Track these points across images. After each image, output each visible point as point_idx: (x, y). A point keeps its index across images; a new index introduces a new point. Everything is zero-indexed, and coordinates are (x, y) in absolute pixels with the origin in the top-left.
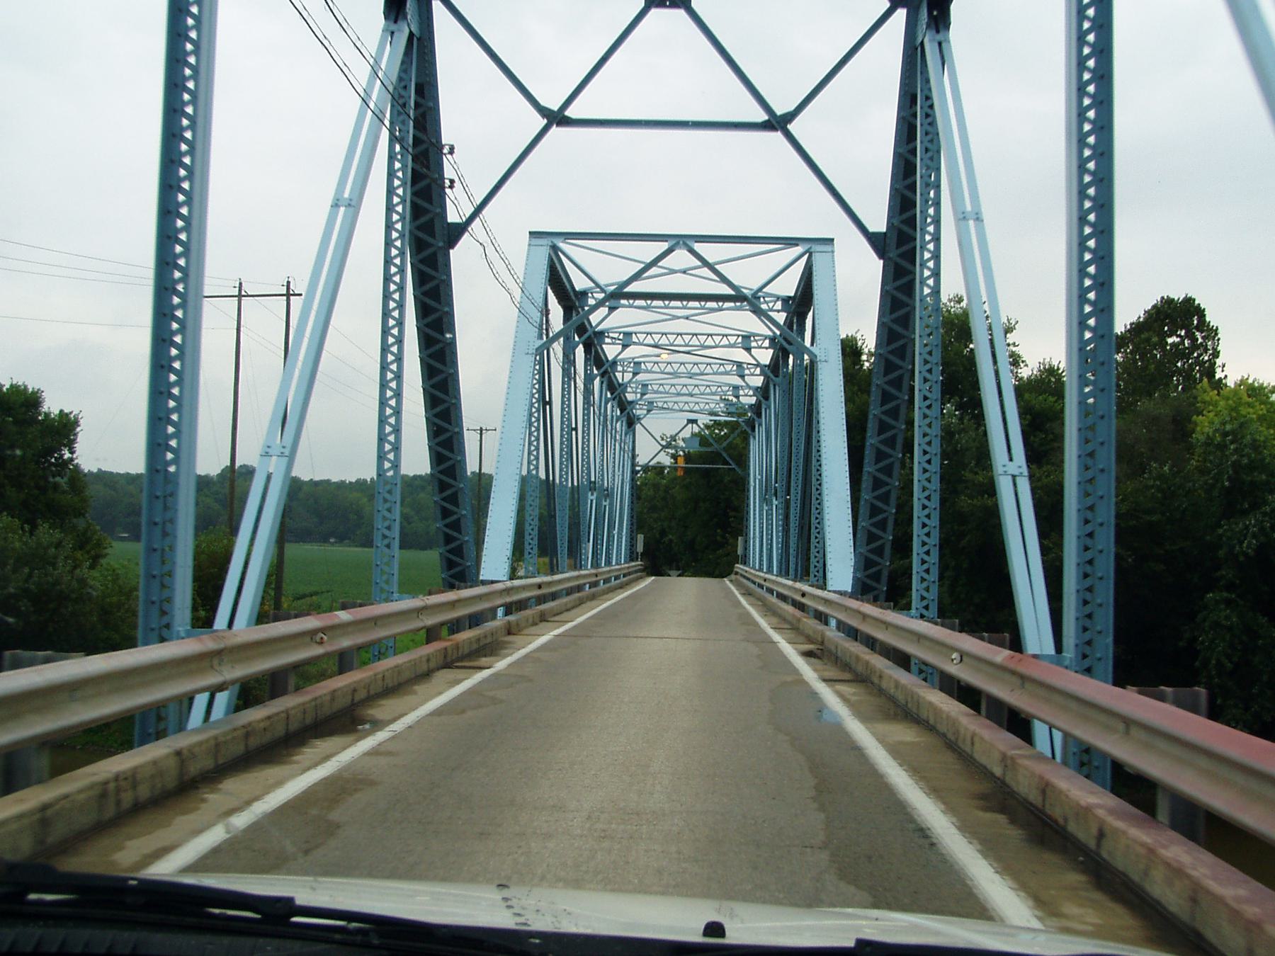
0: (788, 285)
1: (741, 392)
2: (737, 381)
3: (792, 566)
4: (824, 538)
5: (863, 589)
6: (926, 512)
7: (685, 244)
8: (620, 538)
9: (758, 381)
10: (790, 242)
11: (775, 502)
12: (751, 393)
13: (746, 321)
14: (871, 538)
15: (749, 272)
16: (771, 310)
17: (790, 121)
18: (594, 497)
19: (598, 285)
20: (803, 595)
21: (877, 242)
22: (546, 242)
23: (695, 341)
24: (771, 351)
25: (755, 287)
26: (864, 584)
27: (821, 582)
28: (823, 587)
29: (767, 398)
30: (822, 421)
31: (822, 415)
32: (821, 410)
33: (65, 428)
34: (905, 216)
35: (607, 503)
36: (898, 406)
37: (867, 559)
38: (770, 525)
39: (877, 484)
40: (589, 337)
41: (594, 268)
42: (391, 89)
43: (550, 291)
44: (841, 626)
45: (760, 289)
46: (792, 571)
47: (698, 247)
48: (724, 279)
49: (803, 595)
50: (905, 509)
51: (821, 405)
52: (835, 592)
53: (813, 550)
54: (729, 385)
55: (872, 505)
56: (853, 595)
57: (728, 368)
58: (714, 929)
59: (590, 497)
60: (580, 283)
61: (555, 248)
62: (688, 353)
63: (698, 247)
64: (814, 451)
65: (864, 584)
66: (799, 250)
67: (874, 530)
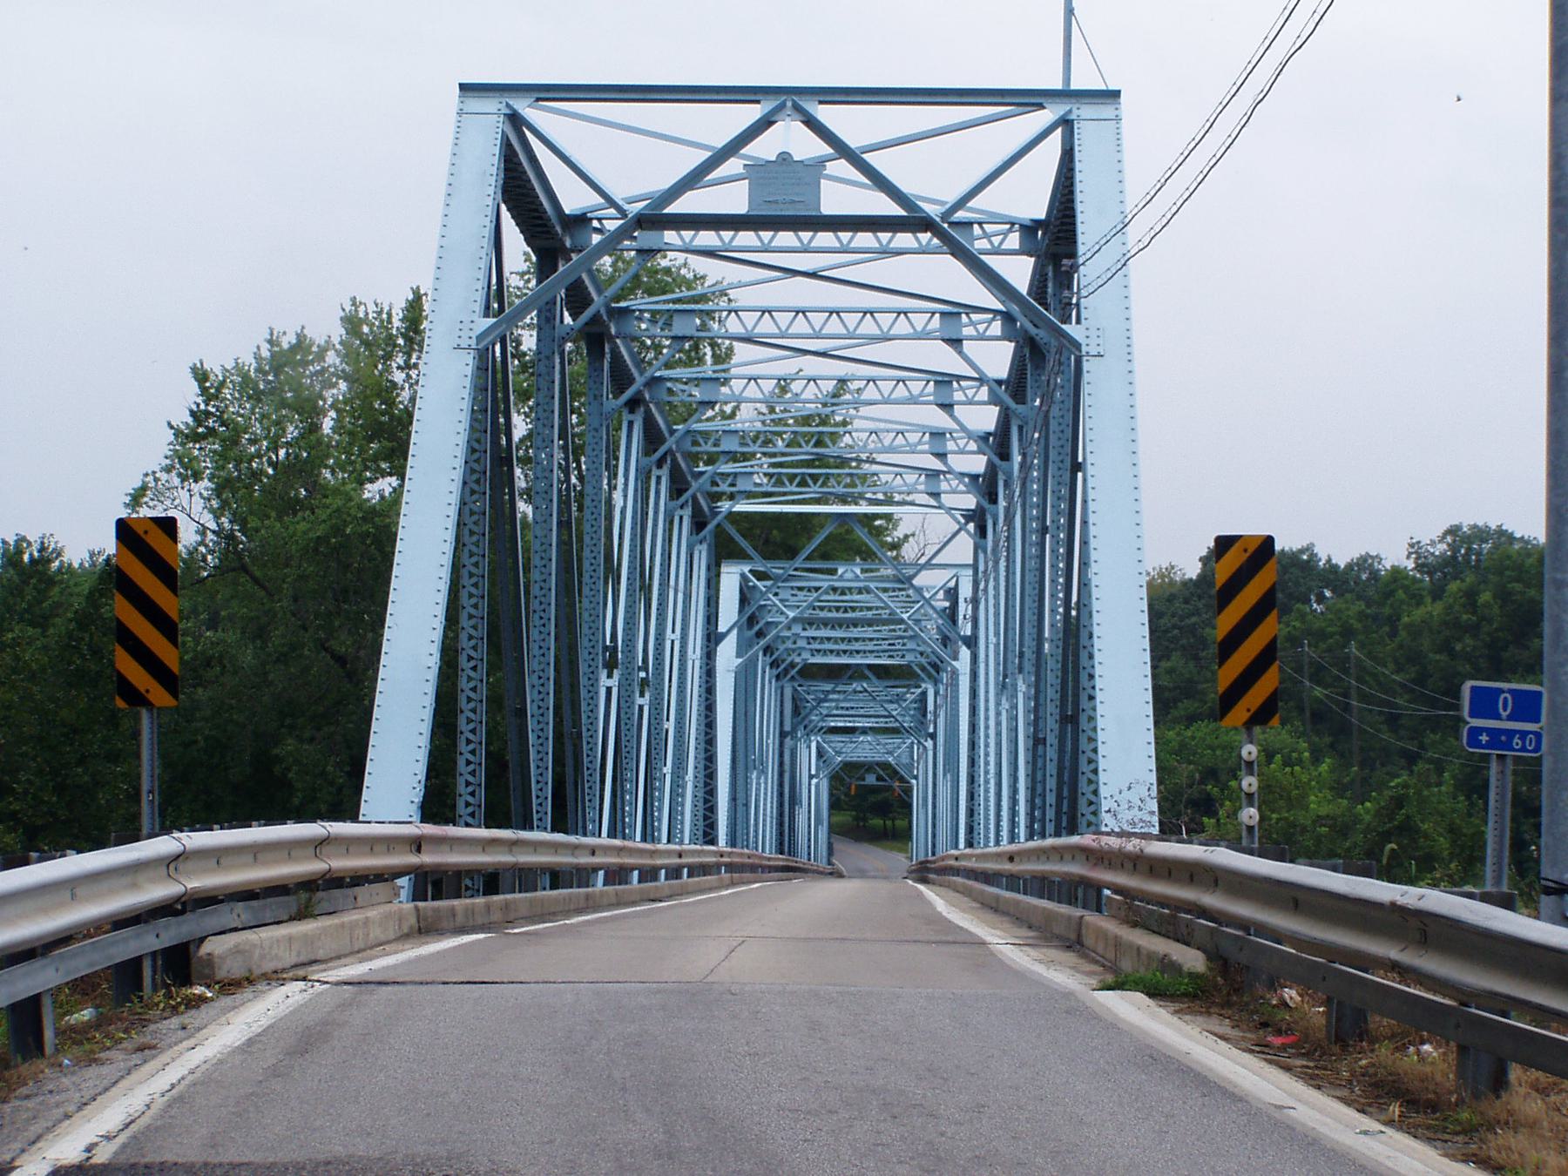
0: (1028, 194)
1: (951, 446)
2: (940, 419)
7: (798, 109)
8: (678, 784)
9: (986, 418)
10: (1029, 99)
11: (1022, 687)
12: (984, 393)
13: (949, 278)
15: (934, 171)
16: (997, 252)
18: (613, 682)
19: (611, 202)
22: (492, 105)
23: (834, 326)
24: (1009, 348)
25: (951, 198)
28: (1094, 827)
29: (1005, 456)
35: (645, 701)
40: (596, 318)
41: (607, 164)
42: (710, 979)
43: (506, 215)
45: (961, 203)
47: (826, 114)
48: (880, 182)
50: (1020, 440)
54: (923, 430)
57: (916, 387)
59: (604, 681)
60: (572, 197)
61: (515, 120)
62: (824, 354)
63: (826, 114)
66: (1046, 116)
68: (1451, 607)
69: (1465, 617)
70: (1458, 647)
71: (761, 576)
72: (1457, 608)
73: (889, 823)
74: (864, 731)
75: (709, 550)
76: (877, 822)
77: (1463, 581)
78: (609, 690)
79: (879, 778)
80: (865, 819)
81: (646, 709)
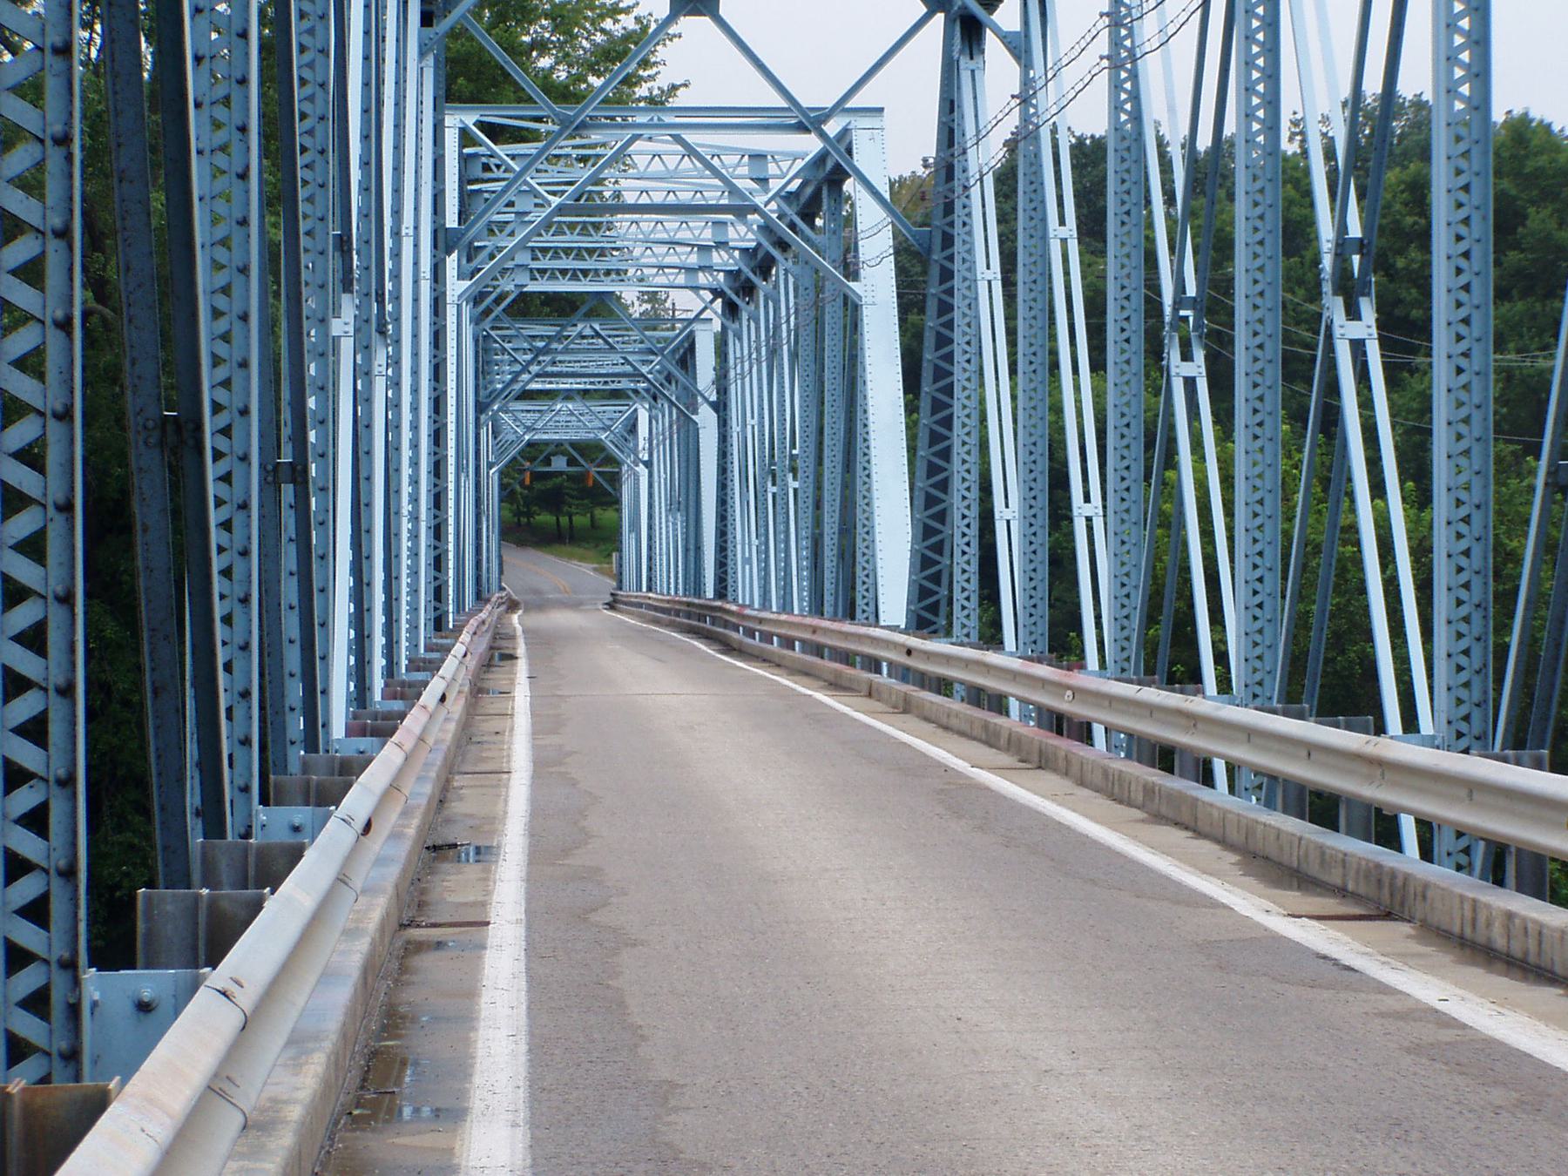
3: (828, 599)
4: (875, 570)
6: (966, 594)
17: (825, 122)
18: (1366, 327)
20: (909, 652)
26: (920, 618)
27: (872, 618)
28: (876, 624)
30: (871, 410)
31: (870, 402)
33: (1549, 125)
34: (944, 287)
36: (938, 602)
37: (926, 526)
53: (860, 588)
55: (938, 333)
58: (198, 813)
59: (1346, 331)
64: (859, 439)
68: (1388, 206)
69: (1409, 220)
70: (1400, 263)
71: (496, 132)
72: (1398, 207)
73: (564, 520)
74: (568, 395)
75: (436, 67)
76: (545, 518)
77: (1405, 168)
78: (1190, 383)
79: (572, 462)
80: (529, 515)
81: (1098, 524)
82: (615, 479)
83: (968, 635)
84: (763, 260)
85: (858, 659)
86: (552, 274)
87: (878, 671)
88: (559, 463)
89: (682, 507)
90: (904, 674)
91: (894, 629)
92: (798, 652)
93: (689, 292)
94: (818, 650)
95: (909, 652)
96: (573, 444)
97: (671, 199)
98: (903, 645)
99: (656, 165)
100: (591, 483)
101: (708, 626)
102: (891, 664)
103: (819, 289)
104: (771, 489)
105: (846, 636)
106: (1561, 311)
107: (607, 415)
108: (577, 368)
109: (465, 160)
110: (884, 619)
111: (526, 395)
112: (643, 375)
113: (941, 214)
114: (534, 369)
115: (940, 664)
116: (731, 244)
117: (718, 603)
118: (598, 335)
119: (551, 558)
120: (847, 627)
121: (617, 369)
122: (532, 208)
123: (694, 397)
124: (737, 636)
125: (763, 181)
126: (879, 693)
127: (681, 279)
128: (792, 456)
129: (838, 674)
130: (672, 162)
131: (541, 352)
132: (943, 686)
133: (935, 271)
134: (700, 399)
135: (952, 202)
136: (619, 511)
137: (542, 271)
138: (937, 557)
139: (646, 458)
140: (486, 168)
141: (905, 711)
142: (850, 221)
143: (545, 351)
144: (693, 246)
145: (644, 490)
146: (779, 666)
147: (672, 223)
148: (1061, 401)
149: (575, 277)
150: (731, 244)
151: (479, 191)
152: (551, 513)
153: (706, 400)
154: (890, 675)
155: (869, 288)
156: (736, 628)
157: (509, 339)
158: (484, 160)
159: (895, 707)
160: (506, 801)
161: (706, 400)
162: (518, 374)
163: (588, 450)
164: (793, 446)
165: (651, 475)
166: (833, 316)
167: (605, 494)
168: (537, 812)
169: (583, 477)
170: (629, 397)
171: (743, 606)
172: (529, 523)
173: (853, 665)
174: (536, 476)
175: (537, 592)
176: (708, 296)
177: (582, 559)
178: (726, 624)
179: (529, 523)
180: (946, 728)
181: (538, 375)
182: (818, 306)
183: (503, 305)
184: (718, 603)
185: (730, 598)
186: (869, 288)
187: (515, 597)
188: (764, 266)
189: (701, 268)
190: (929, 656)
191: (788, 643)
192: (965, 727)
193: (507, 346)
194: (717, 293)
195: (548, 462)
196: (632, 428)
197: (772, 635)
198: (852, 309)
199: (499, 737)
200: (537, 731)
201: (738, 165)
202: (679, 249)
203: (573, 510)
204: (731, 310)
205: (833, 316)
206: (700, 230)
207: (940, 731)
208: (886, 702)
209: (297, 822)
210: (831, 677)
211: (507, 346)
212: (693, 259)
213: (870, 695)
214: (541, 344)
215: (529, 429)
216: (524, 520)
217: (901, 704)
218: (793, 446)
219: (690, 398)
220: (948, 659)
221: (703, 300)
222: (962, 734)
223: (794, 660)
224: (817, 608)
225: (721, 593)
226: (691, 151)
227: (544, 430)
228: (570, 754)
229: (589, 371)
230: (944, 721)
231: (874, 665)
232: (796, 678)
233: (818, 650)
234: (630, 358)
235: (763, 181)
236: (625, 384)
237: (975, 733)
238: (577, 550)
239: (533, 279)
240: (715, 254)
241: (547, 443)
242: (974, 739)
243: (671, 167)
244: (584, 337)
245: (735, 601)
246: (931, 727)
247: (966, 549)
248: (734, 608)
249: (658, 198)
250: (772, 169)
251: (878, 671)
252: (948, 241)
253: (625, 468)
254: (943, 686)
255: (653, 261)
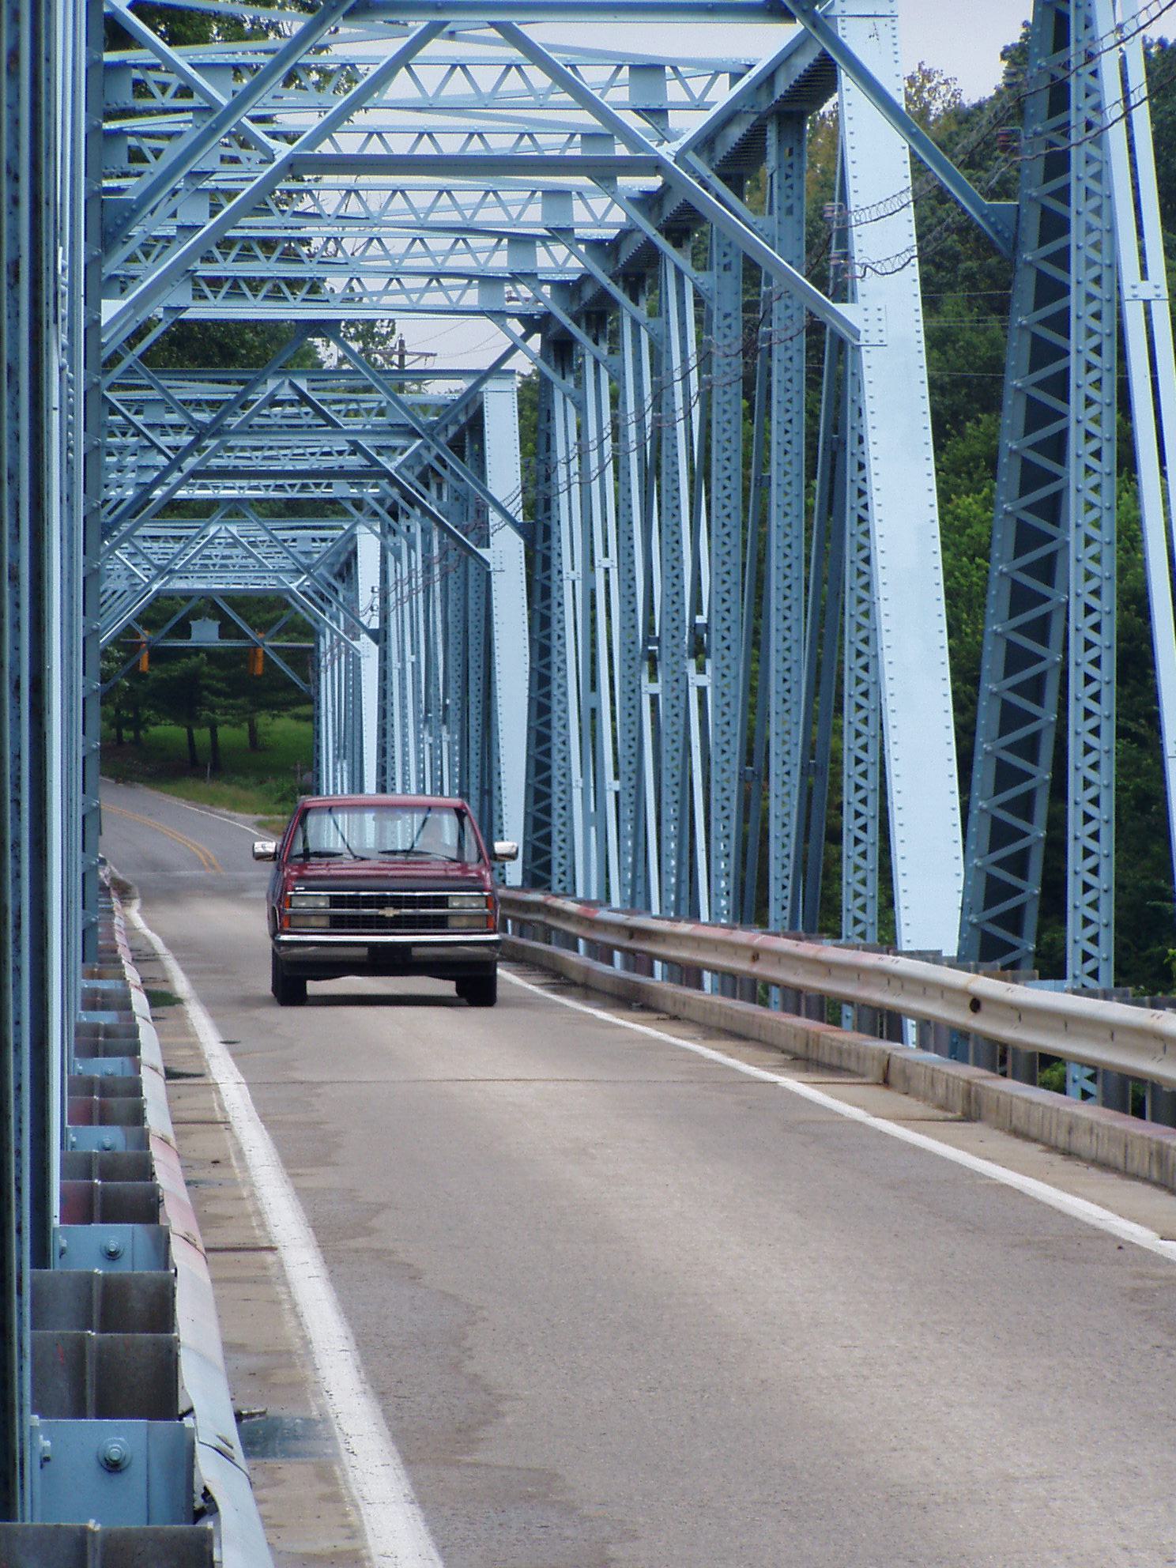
5: (987, 947)
11: (445, 736)
14: (1001, 834)
20: (976, 1005)
21: (521, 529)
28: (888, 941)
32: (869, 406)
37: (991, 880)
38: (436, 768)
39: (1011, 718)
44: (930, 1032)
46: (779, 893)
49: (755, 958)
51: (868, 390)
52: (911, 955)
56: (959, 962)
65: (534, 875)
67: (1005, 816)
73: (202, 735)
74: (235, 509)
76: (167, 731)
79: (227, 629)
80: (137, 724)
82: (306, 661)
83: (863, 935)
84: (633, 260)
85: (848, 1011)
86: (236, 288)
87: (896, 1034)
88: (205, 633)
89: (454, 716)
90: (957, 1043)
91: (934, 957)
92: (708, 990)
93: (486, 323)
94: (755, 990)
95: (755, 958)
96: (230, 597)
97: (476, 147)
98: (964, 992)
99: (458, 85)
100: (259, 668)
101: (510, 935)
102: (926, 1024)
103: (754, 312)
104: (648, 688)
105: (829, 968)
106: (927, 315)
107: (301, 546)
108: (257, 462)
109: (101, 75)
110: (909, 936)
111: (174, 508)
112: (387, 474)
113: (1039, 175)
114: (190, 463)
115: (914, 995)
116: (579, 232)
117: (536, 897)
118: (304, 399)
119: (176, 802)
120: (828, 951)
121: (333, 462)
122: (216, 164)
123: (481, 513)
124: (579, 958)
125: (656, 114)
126: (907, 1079)
127: (472, 297)
128: (694, 627)
129: (809, 1039)
130: (485, 78)
131: (202, 432)
132: (1043, 1068)
133: (1025, 287)
134: (494, 517)
135: (1066, 154)
136: (314, 719)
137: (215, 282)
138: (1020, 824)
139: (375, 624)
140: (140, 88)
141: (968, 1117)
142: (834, 185)
143: (216, 430)
144: (500, 235)
145: (370, 679)
146: (675, 1018)
147: (468, 192)
148: (1139, 521)
149: (275, 295)
150: (579, 232)
151: (119, 133)
152: (177, 721)
153: (509, 519)
154: (922, 1044)
155: (872, 315)
156: (571, 943)
157: (139, 407)
158: (136, 74)
159: (943, 1107)
160: (298, 1316)
161: (509, 519)
162: (166, 472)
163: (264, 608)
164: (697, 609)
165: (384, 656)
166: (786, 369)
167: (289, 685)
168: (372, 1347)
169: (245, 656)
170: (345, 513)
171: (586, 902)
172: (137, 741)
173: (836, 1022)
174: (159, 655)
175: (155, 865)
176: (518, 329)
177: (235, 805)
178: (547, 933)
179: (137, 741)
180: (1068, 1153)
181: (194, 474)
182: (753, 349)
183: (142, 347)
184: (536, 897)
185: (557, 887)
186: (872, 315)
187: (121, 877)
188: (638, 270)
189: (515, 278)
190: (1021, 1013)
191: (689, 975)
192: (1116, 1155)
193: (138, 419)
194: (533, 324)
195: (183, 630)
196: (347, 570)
197: (652, 957)
198: (830, 357)
199: (216, 1173)
200: (292, 1162)
201: (610, 84)
202: (475, 241)
203: (218, 716)
204: (560, 350)
205: (786, 369)
206: (519, 205)
207: (1057, 1159)
208: (924, 1098)
209: (115, 1451)
210: (798, 1047)
211: (138, 419)
212: (501, 261)
213: (886, 1082)
214: (204, 417)
215: (163, 571)
216: (128, 735)
217: (959, 1102)
218: (697, 609)
219: (474, 512)
220: (1066, 1022)
221: (509, 333)
222: (1104, 1165)
223: (709, 1009)
224: (751, 907)
225: (539, 872)
226: (535, 55)
227: (183, 573)
228: (380, 1208)
229: (276, 466)
230: (1062, 1140)
231: (888, 1023)
232: (716, 1044)
233: (755, 990)
234: (364, 442)
235: (656, 114)
236: (340, 489)
237: (1134, 1166)
238: (229, 790)
239: (200, 296)
240: (540, 251)
241: (187, 596)
242: (1135, 1177)
243: (486, 87)
244: (281, 403)
245: (569, 892)
246: (1033, 1150)
247: (1092, 810)
248: (571, 906)
249: (451, 145)
250: (674, 91)
251: (897, 1035)
252: (1055, 225)
253: (325, 643)
254: (1043, 1068)
255: (426, 263)
